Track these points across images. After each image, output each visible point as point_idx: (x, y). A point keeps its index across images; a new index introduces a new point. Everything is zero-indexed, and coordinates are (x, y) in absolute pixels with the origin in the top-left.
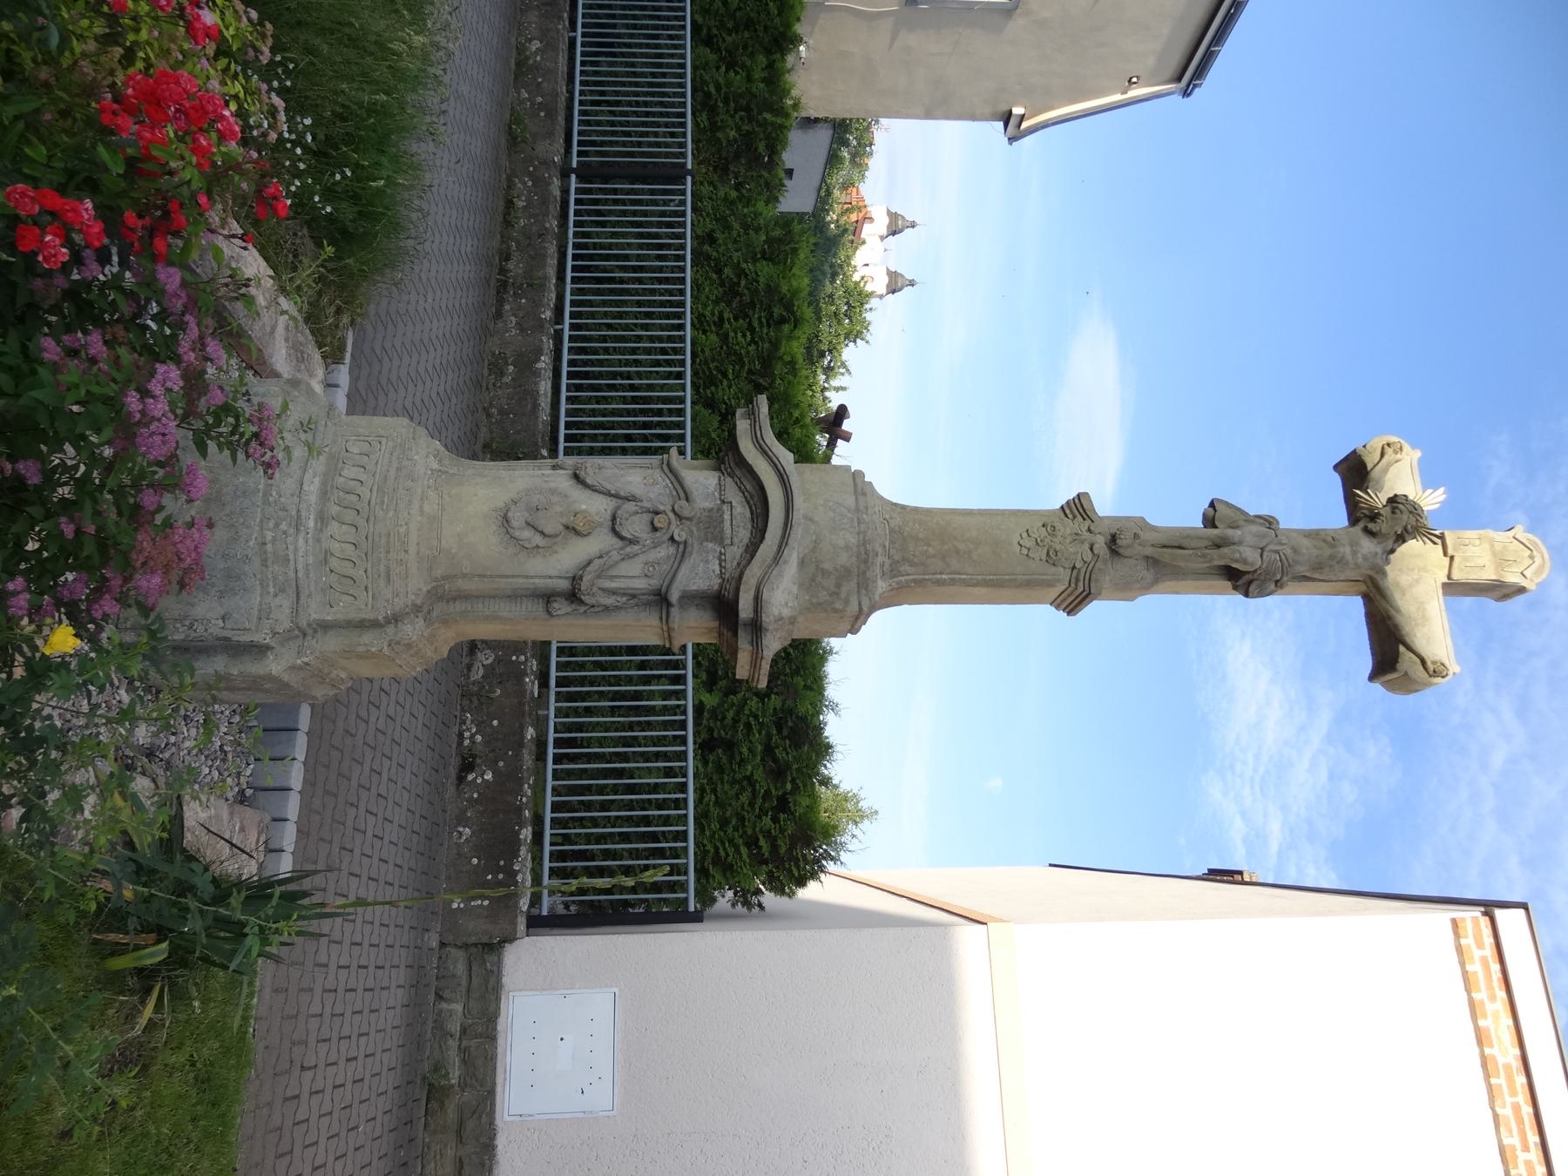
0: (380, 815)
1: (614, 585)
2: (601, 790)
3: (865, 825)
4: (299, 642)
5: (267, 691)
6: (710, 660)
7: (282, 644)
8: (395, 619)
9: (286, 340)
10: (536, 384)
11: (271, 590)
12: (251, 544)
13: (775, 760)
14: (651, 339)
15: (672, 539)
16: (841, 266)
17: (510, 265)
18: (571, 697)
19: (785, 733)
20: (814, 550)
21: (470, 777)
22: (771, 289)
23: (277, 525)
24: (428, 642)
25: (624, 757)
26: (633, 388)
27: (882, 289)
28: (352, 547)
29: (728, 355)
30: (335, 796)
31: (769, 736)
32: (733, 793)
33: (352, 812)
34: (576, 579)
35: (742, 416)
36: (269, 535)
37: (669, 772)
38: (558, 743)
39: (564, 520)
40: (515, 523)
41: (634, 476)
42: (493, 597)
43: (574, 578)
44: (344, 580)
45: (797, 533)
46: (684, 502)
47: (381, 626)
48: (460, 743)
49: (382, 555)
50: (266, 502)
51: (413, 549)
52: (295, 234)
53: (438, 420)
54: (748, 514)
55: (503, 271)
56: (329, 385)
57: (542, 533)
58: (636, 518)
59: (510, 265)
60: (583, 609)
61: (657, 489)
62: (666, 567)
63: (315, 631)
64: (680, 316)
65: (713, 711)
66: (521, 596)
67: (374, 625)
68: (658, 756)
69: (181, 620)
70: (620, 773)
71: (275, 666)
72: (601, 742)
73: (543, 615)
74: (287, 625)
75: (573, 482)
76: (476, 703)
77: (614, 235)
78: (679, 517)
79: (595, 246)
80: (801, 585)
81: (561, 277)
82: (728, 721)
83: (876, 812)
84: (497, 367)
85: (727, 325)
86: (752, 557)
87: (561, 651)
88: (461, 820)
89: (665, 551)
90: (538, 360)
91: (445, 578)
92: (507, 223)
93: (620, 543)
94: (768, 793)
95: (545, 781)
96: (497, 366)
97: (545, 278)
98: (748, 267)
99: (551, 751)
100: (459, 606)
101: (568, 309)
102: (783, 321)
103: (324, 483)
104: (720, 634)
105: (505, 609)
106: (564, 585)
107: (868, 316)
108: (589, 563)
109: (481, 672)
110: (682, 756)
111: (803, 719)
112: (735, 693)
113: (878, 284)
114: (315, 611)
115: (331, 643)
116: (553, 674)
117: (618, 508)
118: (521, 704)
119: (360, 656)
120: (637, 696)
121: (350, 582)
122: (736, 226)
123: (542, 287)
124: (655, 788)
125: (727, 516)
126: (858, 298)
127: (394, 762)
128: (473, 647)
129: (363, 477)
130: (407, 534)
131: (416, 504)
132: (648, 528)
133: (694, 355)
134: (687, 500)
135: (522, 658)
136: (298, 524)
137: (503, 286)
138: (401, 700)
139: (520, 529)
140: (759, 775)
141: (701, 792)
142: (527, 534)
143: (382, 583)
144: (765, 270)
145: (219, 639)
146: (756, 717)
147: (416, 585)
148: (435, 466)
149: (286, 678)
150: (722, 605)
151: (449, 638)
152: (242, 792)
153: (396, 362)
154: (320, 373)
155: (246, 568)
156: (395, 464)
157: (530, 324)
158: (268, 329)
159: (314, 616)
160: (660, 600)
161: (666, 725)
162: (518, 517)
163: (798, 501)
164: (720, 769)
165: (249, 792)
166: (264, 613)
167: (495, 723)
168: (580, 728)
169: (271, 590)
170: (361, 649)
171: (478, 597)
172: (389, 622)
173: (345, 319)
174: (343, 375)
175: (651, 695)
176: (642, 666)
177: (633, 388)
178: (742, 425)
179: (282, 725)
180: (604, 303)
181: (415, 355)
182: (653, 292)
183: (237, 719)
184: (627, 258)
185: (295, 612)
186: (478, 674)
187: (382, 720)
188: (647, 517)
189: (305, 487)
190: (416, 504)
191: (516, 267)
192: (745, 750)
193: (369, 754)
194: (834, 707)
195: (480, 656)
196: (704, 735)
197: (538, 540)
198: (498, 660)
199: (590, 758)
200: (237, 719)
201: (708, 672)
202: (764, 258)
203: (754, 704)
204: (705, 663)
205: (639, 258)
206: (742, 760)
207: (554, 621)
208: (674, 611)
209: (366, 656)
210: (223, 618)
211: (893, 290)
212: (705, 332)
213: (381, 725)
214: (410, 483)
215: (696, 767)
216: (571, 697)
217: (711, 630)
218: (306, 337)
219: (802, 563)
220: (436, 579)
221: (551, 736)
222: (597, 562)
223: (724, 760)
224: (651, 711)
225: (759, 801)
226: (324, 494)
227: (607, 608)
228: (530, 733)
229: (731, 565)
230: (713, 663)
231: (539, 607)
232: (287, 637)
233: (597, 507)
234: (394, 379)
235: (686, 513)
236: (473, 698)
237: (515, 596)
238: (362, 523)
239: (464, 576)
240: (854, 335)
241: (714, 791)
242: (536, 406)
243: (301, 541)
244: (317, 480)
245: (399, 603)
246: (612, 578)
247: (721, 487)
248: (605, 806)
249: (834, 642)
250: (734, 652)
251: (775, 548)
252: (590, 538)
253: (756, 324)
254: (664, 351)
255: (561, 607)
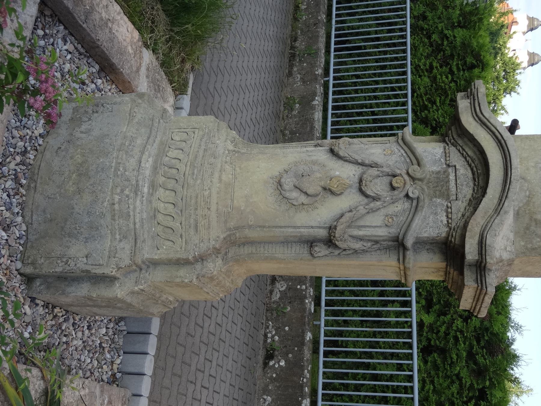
0: (211, 389)
1: (361, 233)
2: (355, 377)
3: (524, 397)
4: (136, 274)
5: (120, 308)
6: (428, 291)
7: (125, 275)
8: (201, 259)
9: (147, 77)
10: (313, 114)
11: (118, 237)
12: (105, 204)
13: (476, 363)
14: (385, 82)
15: (407, 196)
16: (500, 49)
17: (297, 44)
18: (335, 313)
19: (482, 343)
20: (528, 203)
21: (271, 363)
22: (465, 45)
23: (122, 191)
24: (226, 278)
25: (370, 355)
26: (373, 113)
27: (525, 64)
28: (172, 206)
29: (436, 90)
30: (180, 377)
31: (471, 347)
32: (445, 385)
33: (191, 387)
34: (331, 229)
35: (462, 98)
36: (117, 198)
37: (400, 367)
38: (327, 343)
39: (322, 183)
40: (286, 187)
41: (378, 150)
42: (270, 243)
43: (330, 228)
44: (167, 230)
45: (515, 187)
46: (416, 167)
47: (193, 264)
48: (265, 341)
49: (192, 212)
50: (116, 175)
51: (214, 208)
52: (153, 8)
53: (251, 135)
54: (470, 175)
55: (292, 47)
56: (177, 108)
57: (306, 193)
58: (378, 181)
59: (297, 44)
60: (337, 252)
61: (394, 158)
62: (402, 219)
63: (148, 267)
64: (404, 66)
65: (431, 326)
66: (291, 242)
67: (186, 263)
68: (392, 356)
69: (60, 258)
70: (367, 366)
71: (120, 291)
72: (355, 344)
73: (306, 255)
74: (127, 262)
75: (329, 155)
76: (275, 315)
77: (361, 20)
78: (413, 179)
79: (349, 28)
80: (516, 233)
81: (328, 52)
82: (441, 334)
83: (531, 390)
84: (289, 105)
85: (435, 71)
86: (475, 209)
87: (328, 283)
88: (266, 391)
89: (401, 206)
90: (314, 99)
91: (237, 228)
92: (295, 19)
93: (366, 200)
94: (472, 385)
95: (318, 368)
96: (289, 105)
97: (318, 49)
98: (448, 33)
99: (322, 349)
100: (247, 250)
101: (332, 68)
102: (472, 67)
103: (155, 162)
104: (446, 273)
105: (279, 252)
106: (323, 233)
107: (518, 77)
108: (342, 215)
109: (278, 295)
110: (410, 357)
111: (496, 335)
112: (445, 315)
113: (523, 59)
114: (147, 253)
115: (158, 276)
116: (324, 298)
117: (364, 173)
118: (303, 317)
119: (178, 285)
120: (378, 314)
121: (171, 231)
122: (441, 8)
123: (316, 53)
124: (391, 378)
125: (452, 177)
126: (511, 68)
127: (221, 353)
128: (274, 279)
129: (181, 156)
130: (210, 196)
131: (216, 175)
132: (388, 188)
133: (413, 91)
134: (419, 164)
135: (304, 287)
136: (136, 190)
137: (293, 56)
138: (226, 313)
139: (290, 191)
140: (464, 373)
141: (423, 382)
142: (295, 194)
143: (192, 232)
144: (460, 34)
145: (83, 271)
146: (462, 332)
147: (216, 234)
148: (231, 147)
149: (129, 300)
150: (451, 250)
151: (240, 274)
152: (114, 375)
153: (224, 98)
154: (171, 100)
155: (102, 221)
156: (203, 147)
157: (309, 78)
158: (134, 69)
159: (146, 256)
160: (398, 245)
161: (398, 335)
162: (288, 182)
163: (515, 161)
164: (436, 367)
165: (119, 375)
166: (113, 253)
167: (287, 328)
168: (341, 334)
169: (118, 237)
170: (178, 280)
171: (260, 243)
172: (197, 261)
173: (188, 66)
174: (186, 101)
175: (388, 314)
176: (382, 294)
177: (373, 113)
178: (463, 104)
179: (141, 330)
180: (354, 62)
181: (236, 94)
182: (385, 53)
183: (111, 325)
184: (369, 33)
185: (134, 253)
186: (276, 296)
187: (212, 326)
188: (387, 180)
189: (143, 165)
190: (216, 175)
191: (300, 45)
192: (455, 357)
193: (203, 348)
194: (518, 328)
195: (278, 285)
196: (424, 343)
197: (303, 199)
198: (289, 288)
199: (347, 354)
200: (111, 325)
201: (426, 299)
202: (459, 26)
203: (459, 323)
204: (424, 293)
205: (376, 32)
206: (452, 363)
207: (315, 261)
208: (410, 254)
209: (182, 285)
210: (87, 257)
211: (532, 64)
212: (420, 76)
213: (212, 329)
214: (212, 160)
215: (419, 366)
216: (335, 313)
217: (438, 270)
218: (161, 76)
219: (517, 215)
220: (230, 229)
221: (322, 338)
222: (348, 215)
223: (439, 361)
224: (388, 324)
225: (466, 393)
226: (155, 169)
227: (356, 252)
228: (309, 336)
229: (456, 217)
230: (430, 293)
231: (304, 251)
232: (128, 271)
233: (347, 173)
234: (222, 108)
235: (418, 175)
236: (273, 312)
237: (287, 242)
238: (179, 188)
239: (250, 227)
240: (509, 90)
241: (432, 382)
242: (312, 128)
243: (138, 203)
244: (151, 160)
245: (204, 247)
246: (360, 227)
247: (446, 155)
248: (357, 388)
249: (516, 281)
250: (461, 287)
251: (496, 201)
252: (343, 197)
253: (455, 69)
254: (393, 89)
255: (321, 250)
